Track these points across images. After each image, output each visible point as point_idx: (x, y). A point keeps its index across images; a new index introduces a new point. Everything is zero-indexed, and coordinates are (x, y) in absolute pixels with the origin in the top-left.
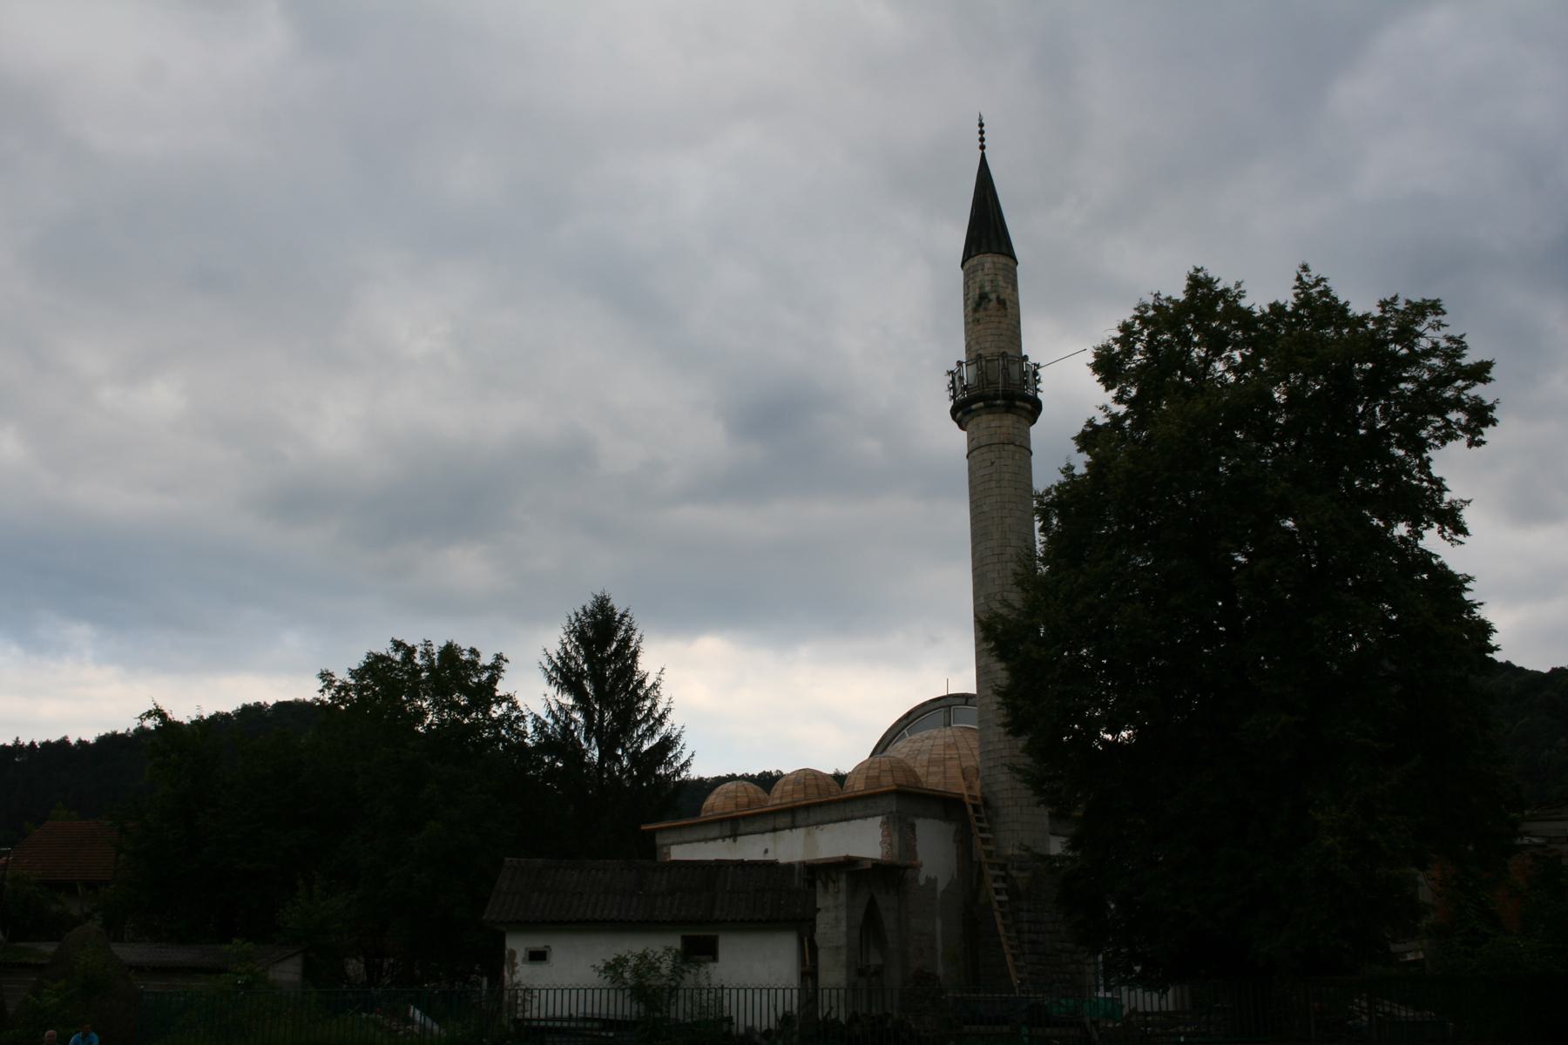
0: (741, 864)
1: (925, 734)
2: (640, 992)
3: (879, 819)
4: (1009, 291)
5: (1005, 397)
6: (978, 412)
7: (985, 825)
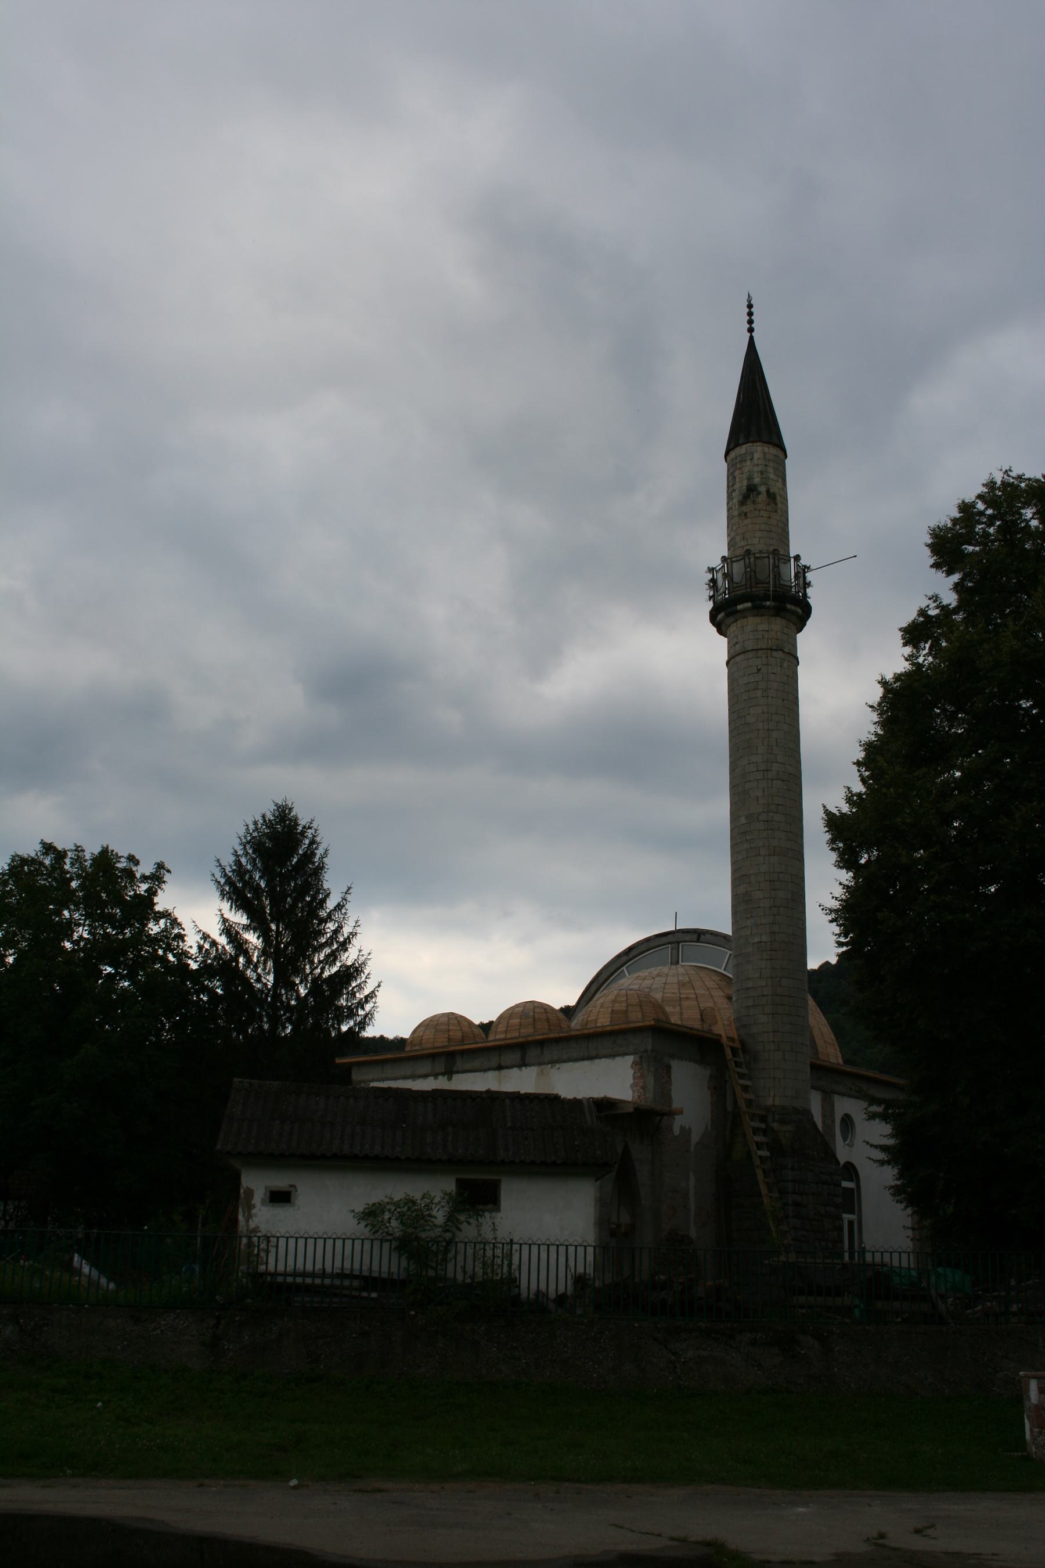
0: (516, 1097)
1: (655, 971)
2: (405, 1245)
3: (630, 1059)
4: (779, 485)
5: (776, 598)
6: (743, 614)
7: (744, 1071)
